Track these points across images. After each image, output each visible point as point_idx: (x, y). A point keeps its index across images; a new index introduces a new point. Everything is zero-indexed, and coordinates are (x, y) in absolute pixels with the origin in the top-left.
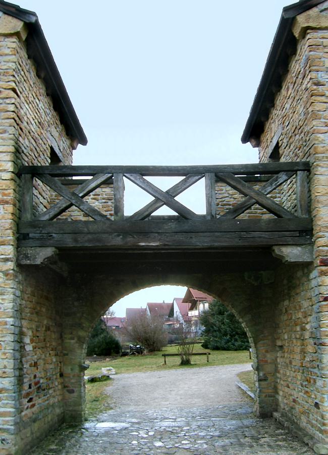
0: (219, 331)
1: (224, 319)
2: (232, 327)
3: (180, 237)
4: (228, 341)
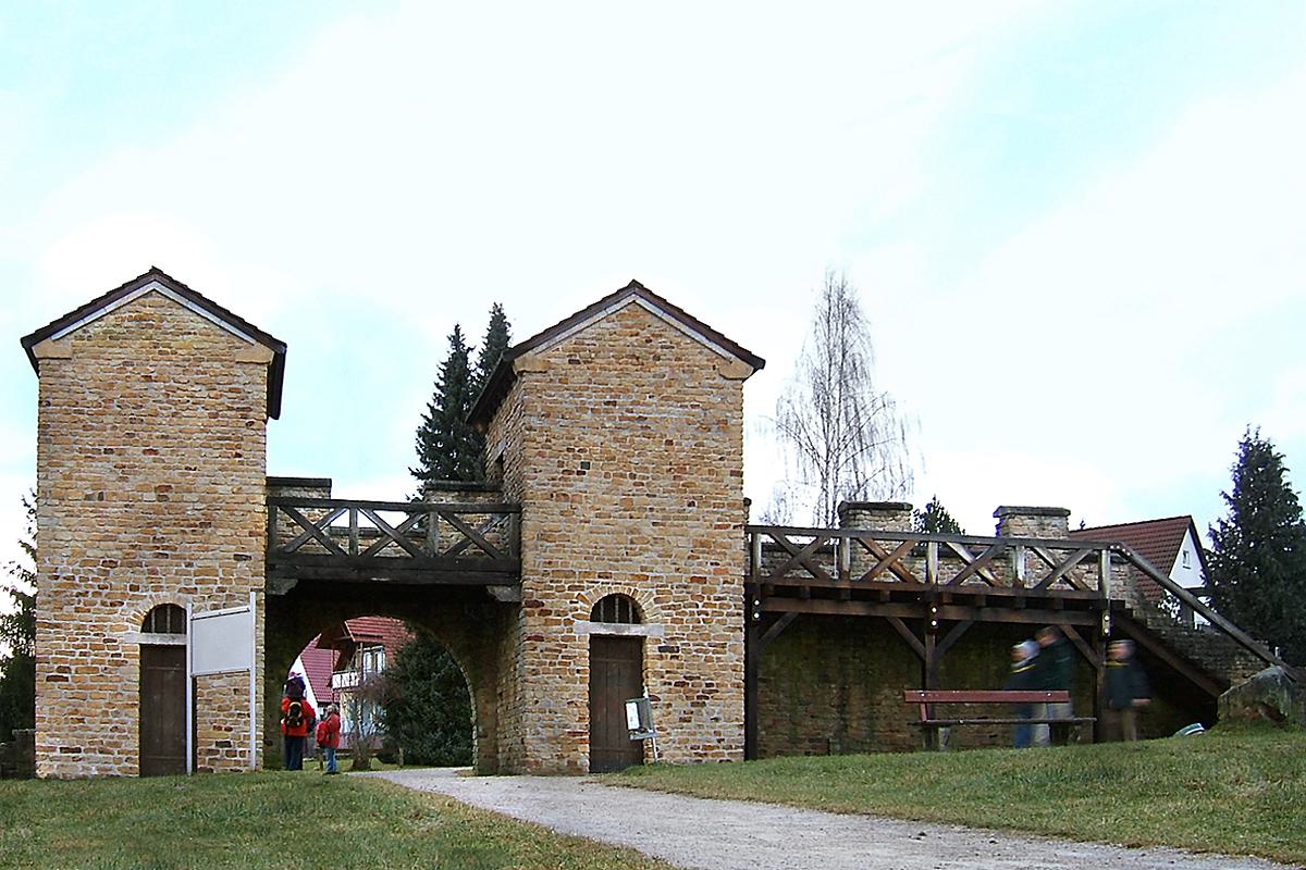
0: (419, 719)
1: (429, 690)
2: (447, 708)
3: (407, 574)
4: (438, 745)
